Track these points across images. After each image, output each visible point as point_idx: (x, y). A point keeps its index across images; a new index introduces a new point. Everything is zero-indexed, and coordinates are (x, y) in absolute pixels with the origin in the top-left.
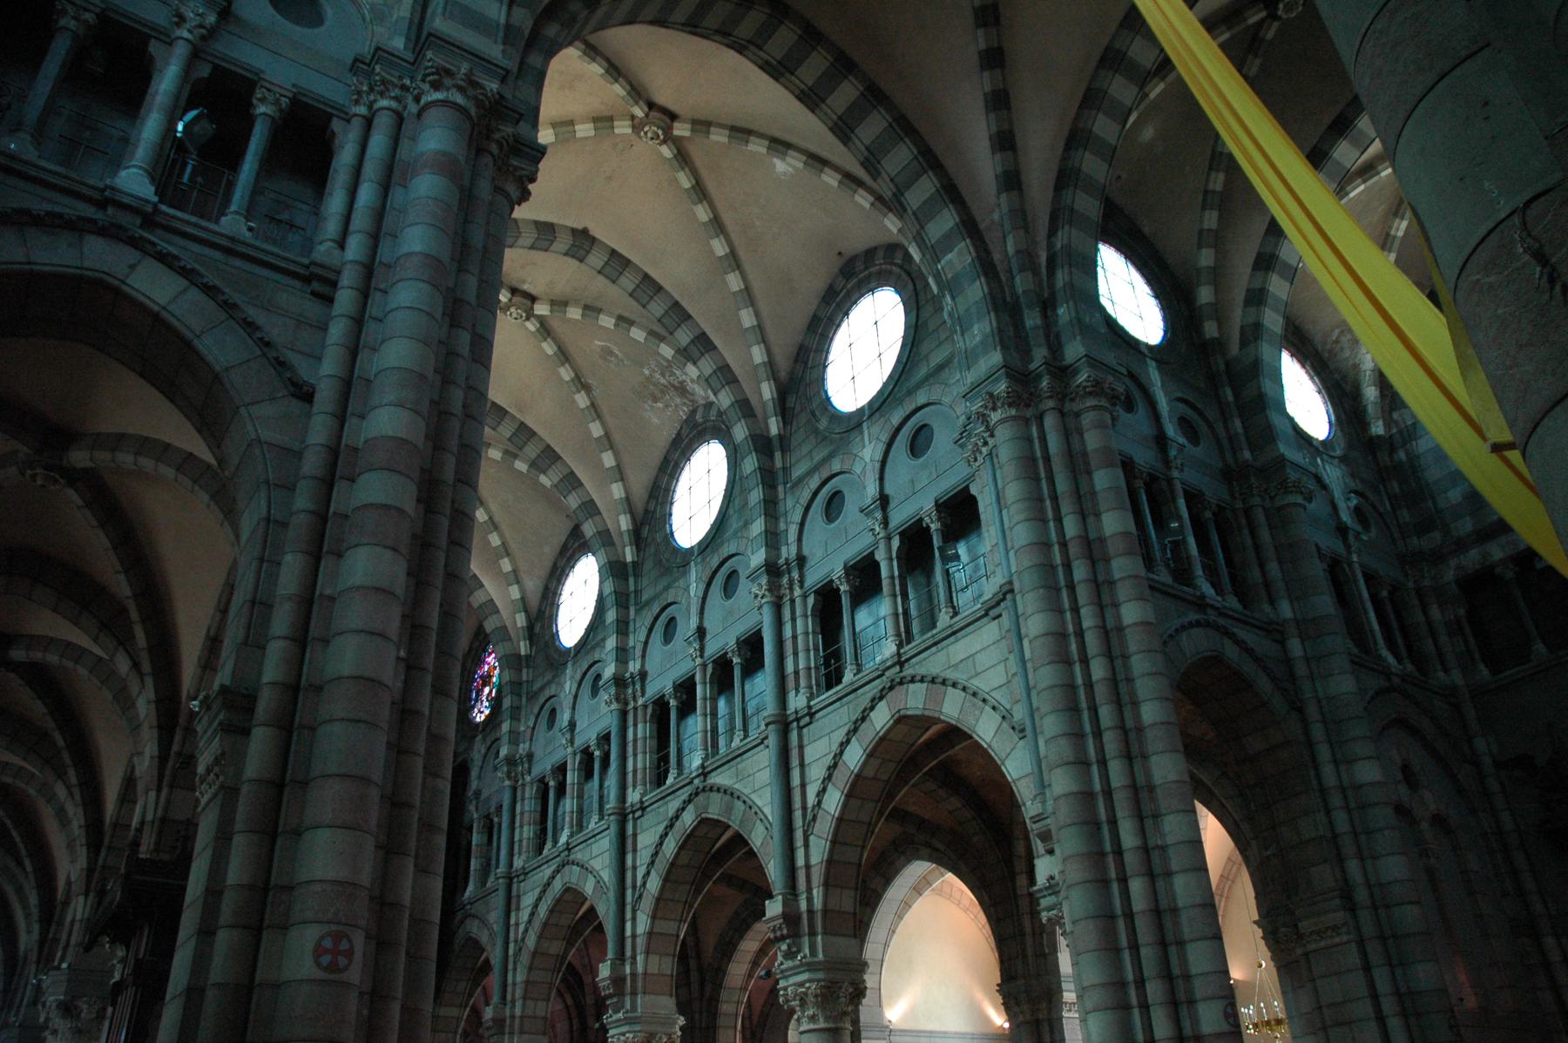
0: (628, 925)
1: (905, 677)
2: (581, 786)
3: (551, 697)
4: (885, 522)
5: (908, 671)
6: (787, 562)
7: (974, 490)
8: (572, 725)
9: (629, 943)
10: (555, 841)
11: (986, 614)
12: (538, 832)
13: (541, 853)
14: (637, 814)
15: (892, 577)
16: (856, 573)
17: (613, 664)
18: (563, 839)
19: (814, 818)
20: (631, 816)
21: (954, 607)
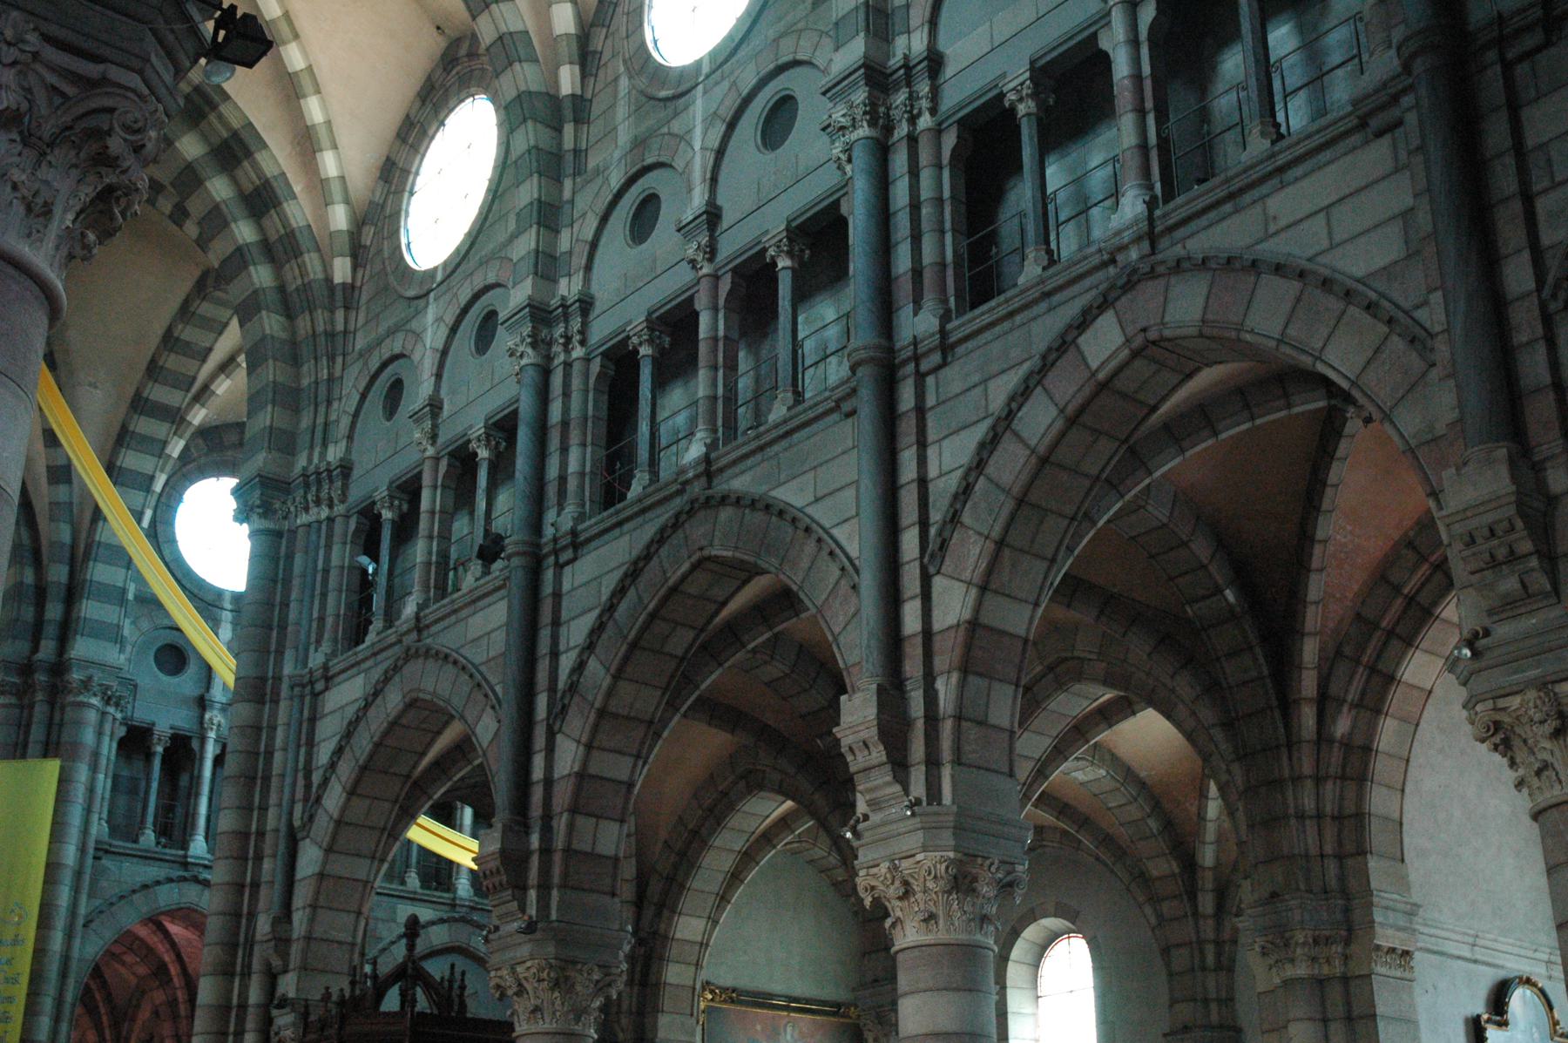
0: (538, 762)
1: (713, 497)
2: (447, 517)
3: (395, 358)
4: (434, 438)
5: (1170, 251)
6: (907, 67)
7: (1104, 44)
8: (435, 406)
9: (537, 794)
10: (390, 617)
11: (837, 407)
12: (356, 605)
13: (359, 640)
14: (564, 557)
15: (939, 201)
16: (403, 496)
17: (529, 282)
18: (410, 609)
19: (943, 545)
20: (551, 559)
21: (1049, 252)
